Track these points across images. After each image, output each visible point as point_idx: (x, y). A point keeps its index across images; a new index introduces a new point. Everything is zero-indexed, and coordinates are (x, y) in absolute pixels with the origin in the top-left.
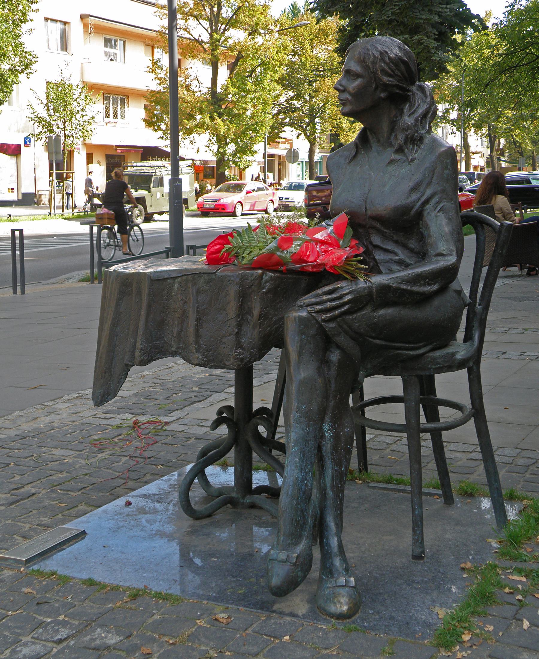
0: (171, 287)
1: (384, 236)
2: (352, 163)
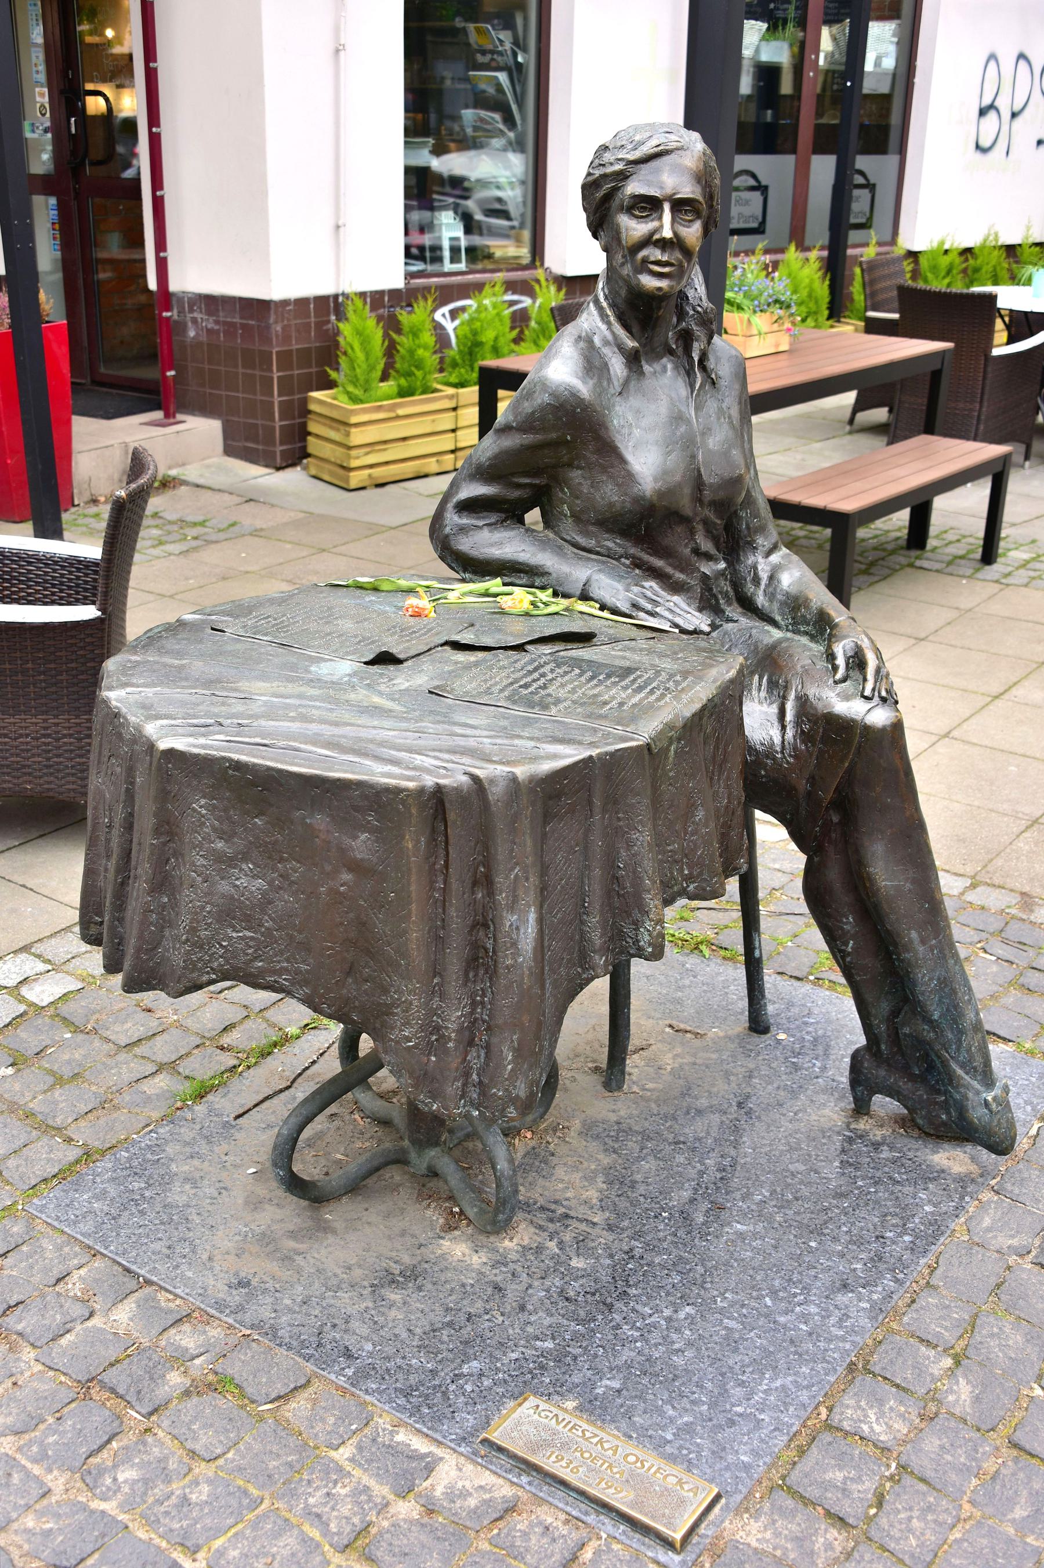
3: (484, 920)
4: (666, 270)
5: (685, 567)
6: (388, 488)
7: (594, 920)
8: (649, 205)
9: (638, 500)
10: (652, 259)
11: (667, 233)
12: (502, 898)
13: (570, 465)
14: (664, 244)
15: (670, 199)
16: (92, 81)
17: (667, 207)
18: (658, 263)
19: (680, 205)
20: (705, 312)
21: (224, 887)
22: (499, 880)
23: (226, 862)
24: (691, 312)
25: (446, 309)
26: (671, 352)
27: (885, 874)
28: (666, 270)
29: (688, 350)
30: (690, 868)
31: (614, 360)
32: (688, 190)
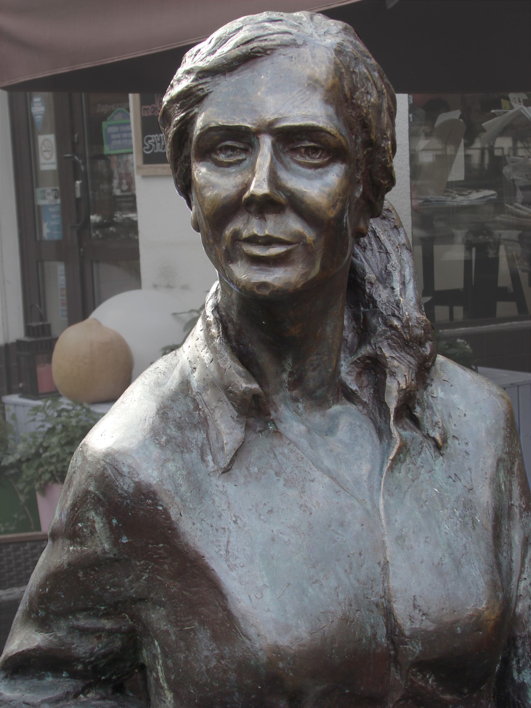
4: (275, 250)
8: (232, 143)
9: (244, 666)
10: (245, 234)
11: (259, 186)
14: (264, 206)
15: (270, 128)
16: (74, 192)
17: (266, 143)
18: (253, 240)
19: (292, 140)
20: (406, 326)
24: (381, 328)
26: (351, 396)
28: (275, 250)
29: (379, 391)
31: (217, 414)
32: (310, 111)
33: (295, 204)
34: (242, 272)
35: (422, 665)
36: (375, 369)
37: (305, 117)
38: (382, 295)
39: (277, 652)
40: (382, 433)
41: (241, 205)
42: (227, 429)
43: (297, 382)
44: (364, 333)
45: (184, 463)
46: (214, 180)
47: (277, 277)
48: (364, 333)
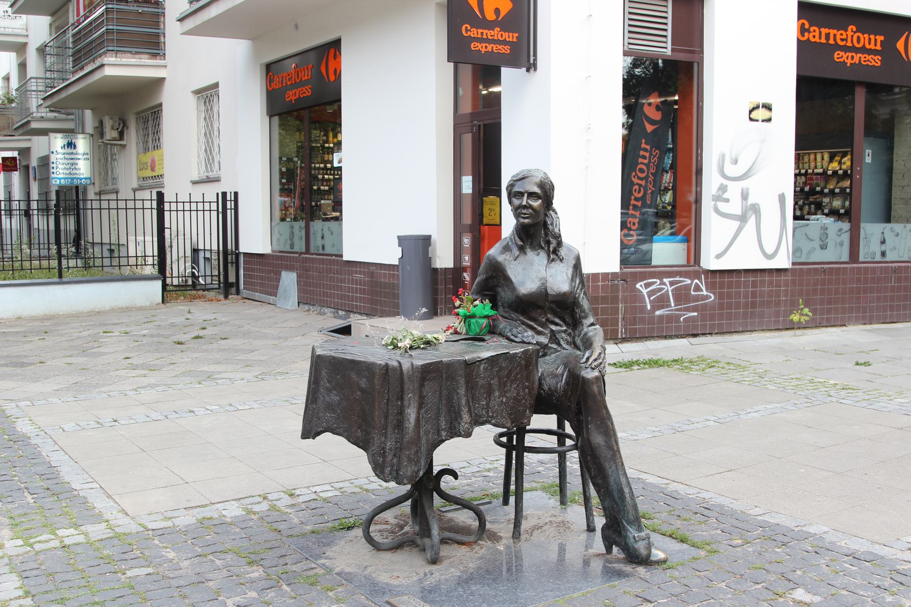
0: (479, 366)
1: (556, 315)
2: (518, 261)
3: (401, 412)
5: (543, 325)
6: (636, 371)
7: (442, 419)
11: (524, 203)
12: (406, 403)
13: (497, 286)
14: (525, 207)
15: (526, 192)
17: (526, 195)
19: (531, 195)
21: (327, 399)
22: (405, 396)
23: (329, 390)
25: (642, 283)
26: (543, 248)
27: (598, 439)
29: (549, 247)
30: (493, 413)
33: (531, 207)
34: (522, 220)
35: (552, 302)
36: (548, 243)
37: (804, 334)
38: (550, 227)
39: (524, 295)
40: (549, 256)
41: (521, 207)
42: (516, 252)
43: (531, 244)
44: (546, 235)
45: (489, 73)
46: (516, 202)
47: (526, 221)
48: (546, 235)
